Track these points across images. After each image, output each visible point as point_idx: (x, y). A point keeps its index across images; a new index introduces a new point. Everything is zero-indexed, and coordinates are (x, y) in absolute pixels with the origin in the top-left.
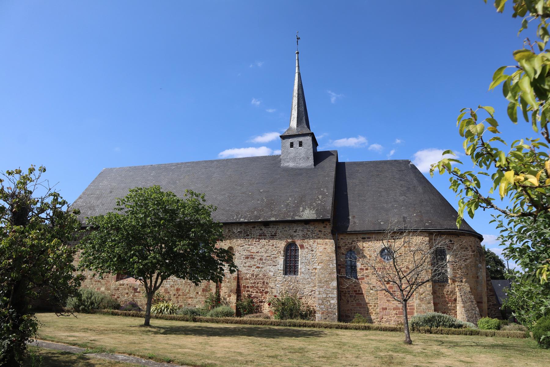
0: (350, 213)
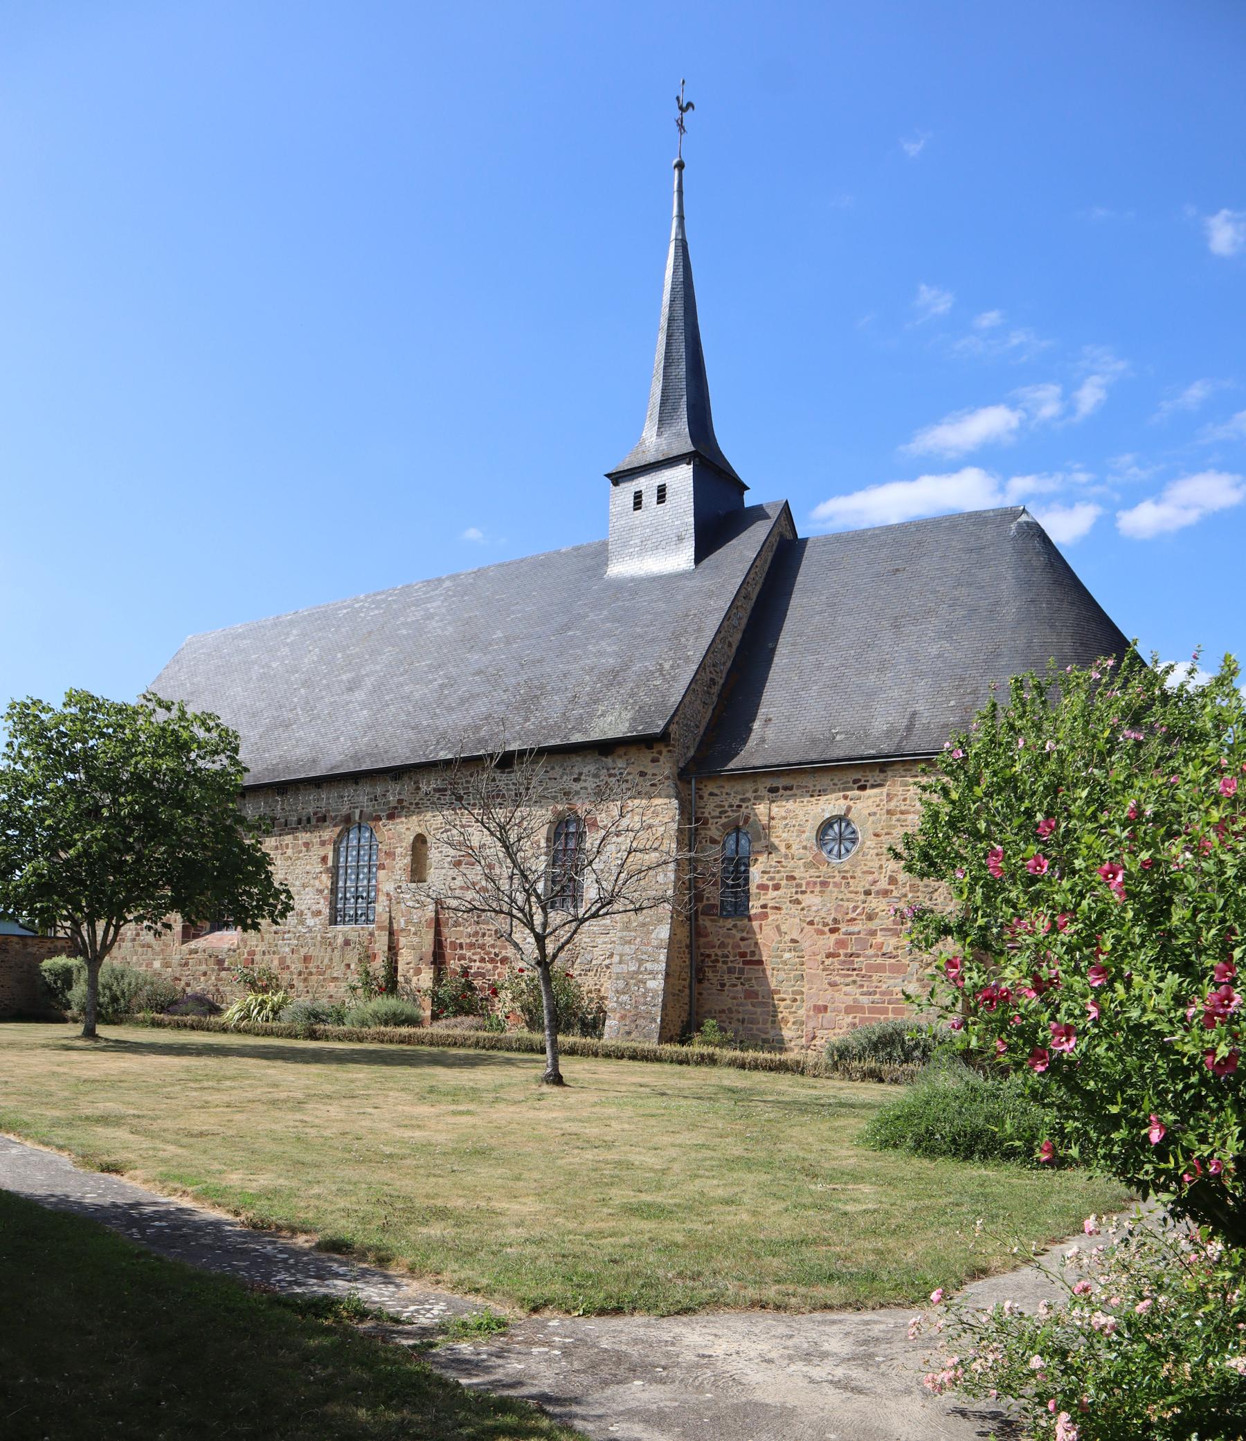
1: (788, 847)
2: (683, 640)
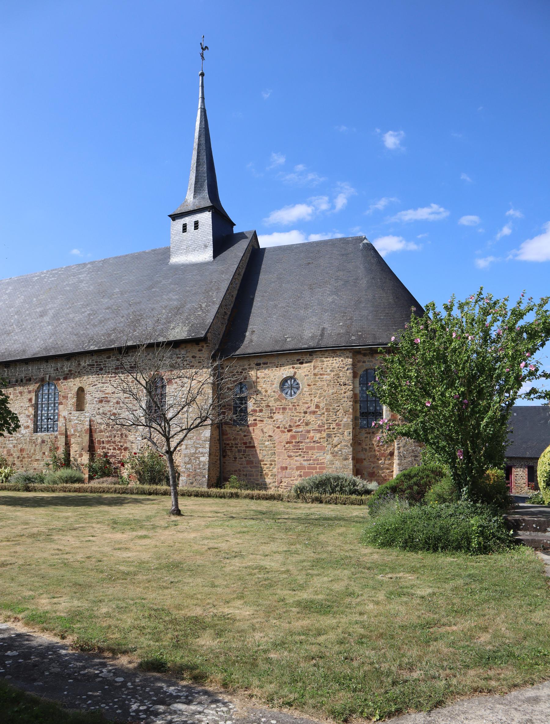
0: (250, 327)
1: (266, 391)
2: (210, 293)
